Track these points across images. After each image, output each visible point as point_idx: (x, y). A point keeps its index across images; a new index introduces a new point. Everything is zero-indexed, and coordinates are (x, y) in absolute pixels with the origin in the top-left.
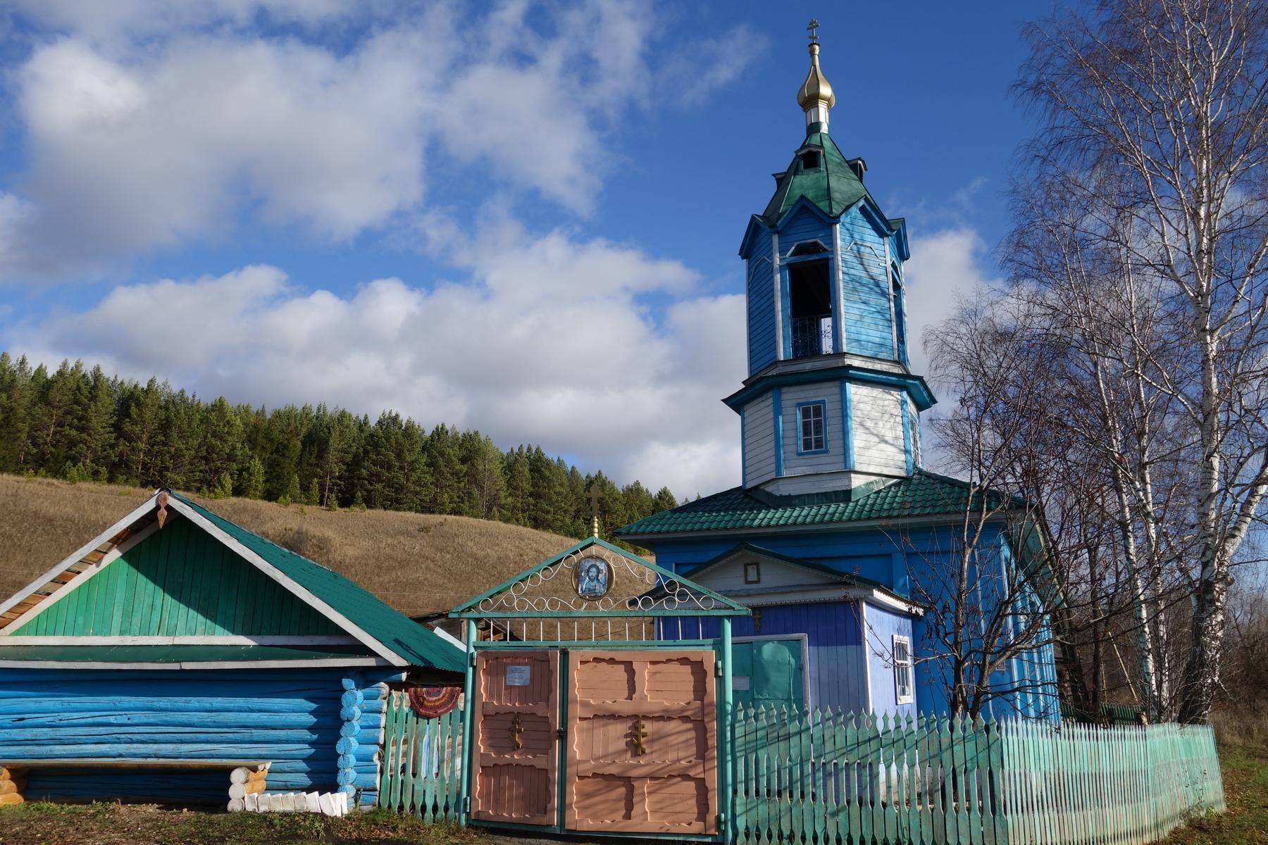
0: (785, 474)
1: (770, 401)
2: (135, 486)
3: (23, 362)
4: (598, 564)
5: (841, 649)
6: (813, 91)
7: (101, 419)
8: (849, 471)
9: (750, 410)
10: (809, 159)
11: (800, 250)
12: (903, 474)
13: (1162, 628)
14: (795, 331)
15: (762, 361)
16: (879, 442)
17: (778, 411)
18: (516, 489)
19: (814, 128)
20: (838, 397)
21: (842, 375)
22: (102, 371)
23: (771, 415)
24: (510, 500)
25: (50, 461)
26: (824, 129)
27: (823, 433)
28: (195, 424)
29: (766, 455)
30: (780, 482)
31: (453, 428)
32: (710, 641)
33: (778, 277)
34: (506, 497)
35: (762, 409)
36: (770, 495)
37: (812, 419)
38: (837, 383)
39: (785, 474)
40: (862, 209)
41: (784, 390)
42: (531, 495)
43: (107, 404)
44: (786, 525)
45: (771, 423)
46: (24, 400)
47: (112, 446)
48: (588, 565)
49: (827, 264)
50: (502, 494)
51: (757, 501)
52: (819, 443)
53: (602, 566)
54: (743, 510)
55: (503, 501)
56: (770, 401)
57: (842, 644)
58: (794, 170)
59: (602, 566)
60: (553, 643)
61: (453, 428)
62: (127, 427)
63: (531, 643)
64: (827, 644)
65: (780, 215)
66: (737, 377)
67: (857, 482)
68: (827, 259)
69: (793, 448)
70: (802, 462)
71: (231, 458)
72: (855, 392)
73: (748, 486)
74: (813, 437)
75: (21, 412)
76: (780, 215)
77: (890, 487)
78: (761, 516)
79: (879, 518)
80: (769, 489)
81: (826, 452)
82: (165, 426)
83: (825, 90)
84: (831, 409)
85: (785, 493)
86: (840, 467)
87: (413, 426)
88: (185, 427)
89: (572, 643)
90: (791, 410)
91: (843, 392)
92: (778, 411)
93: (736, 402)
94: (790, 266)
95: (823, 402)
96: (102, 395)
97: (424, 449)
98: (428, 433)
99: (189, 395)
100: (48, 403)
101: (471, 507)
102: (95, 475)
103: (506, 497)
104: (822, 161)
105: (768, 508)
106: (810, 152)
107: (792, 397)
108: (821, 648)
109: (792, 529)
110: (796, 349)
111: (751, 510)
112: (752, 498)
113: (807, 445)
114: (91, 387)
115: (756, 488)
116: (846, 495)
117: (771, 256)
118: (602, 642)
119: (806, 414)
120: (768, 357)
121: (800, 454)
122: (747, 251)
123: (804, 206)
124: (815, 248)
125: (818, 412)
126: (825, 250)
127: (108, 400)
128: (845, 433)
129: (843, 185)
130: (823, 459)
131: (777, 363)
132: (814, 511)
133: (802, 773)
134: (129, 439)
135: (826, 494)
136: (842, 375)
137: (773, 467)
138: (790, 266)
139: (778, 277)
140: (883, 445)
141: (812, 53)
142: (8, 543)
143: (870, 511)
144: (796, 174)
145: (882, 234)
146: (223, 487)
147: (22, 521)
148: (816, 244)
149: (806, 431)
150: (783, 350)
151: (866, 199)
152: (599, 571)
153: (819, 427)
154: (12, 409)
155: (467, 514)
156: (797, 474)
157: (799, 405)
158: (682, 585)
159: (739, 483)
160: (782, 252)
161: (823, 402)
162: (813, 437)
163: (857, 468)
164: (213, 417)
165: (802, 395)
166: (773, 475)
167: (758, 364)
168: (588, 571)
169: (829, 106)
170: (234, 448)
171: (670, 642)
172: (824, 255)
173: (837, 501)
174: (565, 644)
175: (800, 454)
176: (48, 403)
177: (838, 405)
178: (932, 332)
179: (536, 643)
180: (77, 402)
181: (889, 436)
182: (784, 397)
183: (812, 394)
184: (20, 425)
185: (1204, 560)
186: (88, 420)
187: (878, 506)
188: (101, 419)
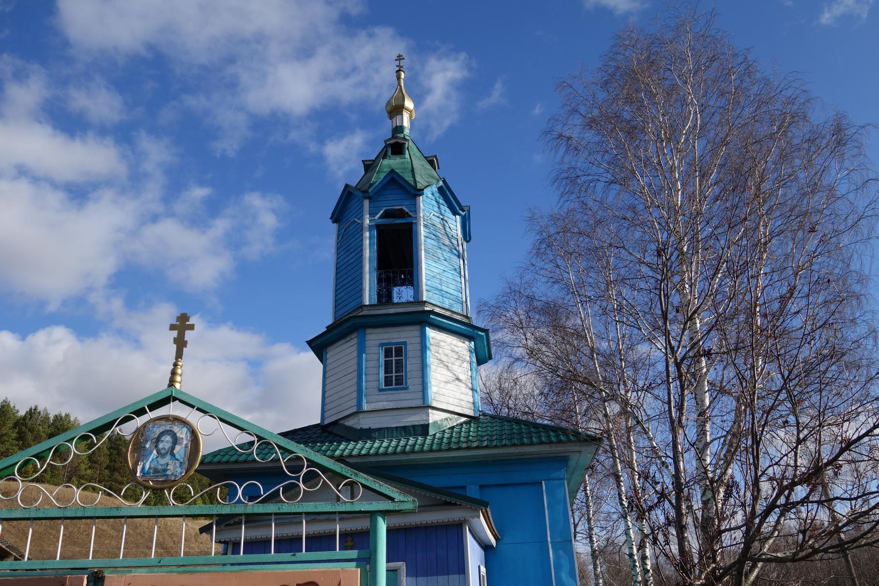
0: (365, 407)
1: (355, 341)
4: (176, 429)
5: (442, 579)
6: (398, 103)
8: (426, 407)
9: (333, 353)
10: (397, 148)
11: (387, 215)
12: (471, 413)
13: (648, 562)
14: (379, 281)
15: (346, 309)
16: (452, 384)
17: (361, 349)
18: (95, 462)
19: (399, 129)
20: (418, 340)
21: (421, 318)
23: (355, 354)
24: (89, 472)
26: (407, 132)
27: (402, 371)
29: (348, 384)
30: (361, 416)
31: (45, 409)
32: (353, 554)
33: (367, 234)
34: (86, 469)
35: (344, 352)
36: (350, 429)
37: (394, 358)
38: (418, 327)
39: (365, 407)
40: (440, 189)
41: (368, 331)
42: (108, 467)
44: (368, 455)
45: (355, 361)
48: (157, 431)
49: (411, 229)
50: (83, 466)
51: (336, 435)
52: (399, 381)
53: (183, 433)
54: (323, 442)
55: (83, 473)
56: (355, 341)
57: (443, 574)
58: (383, 155)
59: (183, 433)
60: (79, 563)
61: (45, 409)
63: (37, 564)
64: (426, 574)
65: (371, 185)
66: (322, 319)
67: (434, 417)
68: (411, 224)
69: (375, 384)
70: (383, 397)
73: (326, 422)
74: (394, 374)
76: (371, 185)
77: (461, 424)
78: (342, 447)
79: (459, 449)
80: (350, 423)
81: (406, 389)
83: (409, 104)
84: (412, 350)
85: (365, 427)
86: (419, 403)
87: (8, 405)
89: (114, 562)
90: (375, 350)
91: (423, 336)
92: (361, 349)
93: (319, 346)
94: (378, 227)
95: (405, 343)
97: (16, 425)
98: (22, 413)
101: (52, 476)
103: (86, 469)
104: (407, 152)
105: (348, 441)
106: (397, 143)
107: (376, 338)
108: (420, 579)
109: (373, 459)
110: (379, 296)
111: (331, 442)
112: (331, 433)
113: (388, 381)
115: (335, 423)
116: (424, 429)
117: (361, 218)
118: (167, 560)
119: (388, 353)
120: (353, 304)
121: (381, 390)
122: (338, 216)
123: (392, 179)
124: (401, 214)
125: (399, 352)
126: (410, 216)
128: (423, 367)
129: (423, 174)
130: (402, 395)
131: (362, 306)
132: (394, 443)
135: (404, 428)
136: (421, 318)
137: (354, 402)
138: (378, 227)
139: (367, 234)
140: (457, 382)
141: (399, 78)
143: (449, 443)
144: (384, 157)
145: (455, 213)
148: (402, 210)
149: (388, 369)
150: (368, 296)
151: (444, 181)
152: (176, 440)
153: (400, 366)
155: (49, 482)
156: (378, 407)
157: (382, 345)
158: (312, 463)
159: (317, 421)
160: (372, 214)
161: (405, 343)
162: (394, 374)
163: (434, 404)
165: (386, 336)
166: (354, 410)
167: (342, 311)
168: (158, 440)
169: (411, 116)
171: (287, 556)
172: (408, 220)
173: (415, 435)
174: (101, 563)
175: (381, 390)
177: (418, 347)
178: (485, 304)
179: (49, 564)
182: (368, 337)
183: (394, 336)
185: (704, 499)
187: (451, 441)
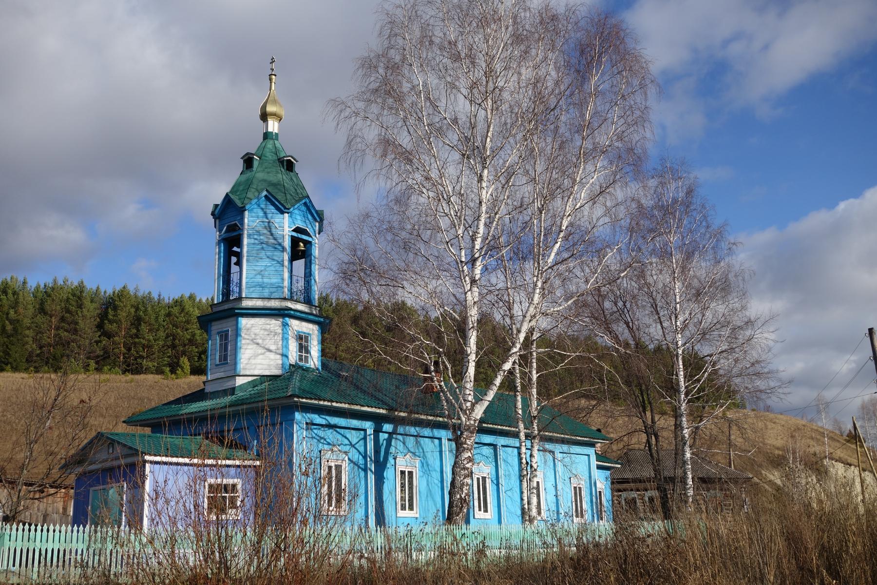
2: (116, 374)
3: (25, 283)
7: (87, 324)
22: (85, 284)
25: (49, 358)
28: (161, 319)
43: (91, 310)
46: (27, 313)
47: (97, 342)
62: (108, 327)
71: (192, 342)
72: (244, 322)
75: (27, 322)
82: (137, 321)
88: (153, 321)
96: (87, 303)
99: (155, 296)
100: (45, 313)
102: (86, 368)
114: (78, 295)
127: (92, 306)
133: (227, 534)
134: (109, 335)
140: (268, 353)
142: (8, 428)
146: (182, 368)
147: (20, 410)
154: (18, 321)
157: (218, 333)
164: (176, 310)
165: (220, 326)
170: (194, 335)
175: (217, 365)
176: (45, 313)
180: (68, 311)
181: (273, 348)
184: (27, 332)
186: (77, 323)
188: (87, 324)
